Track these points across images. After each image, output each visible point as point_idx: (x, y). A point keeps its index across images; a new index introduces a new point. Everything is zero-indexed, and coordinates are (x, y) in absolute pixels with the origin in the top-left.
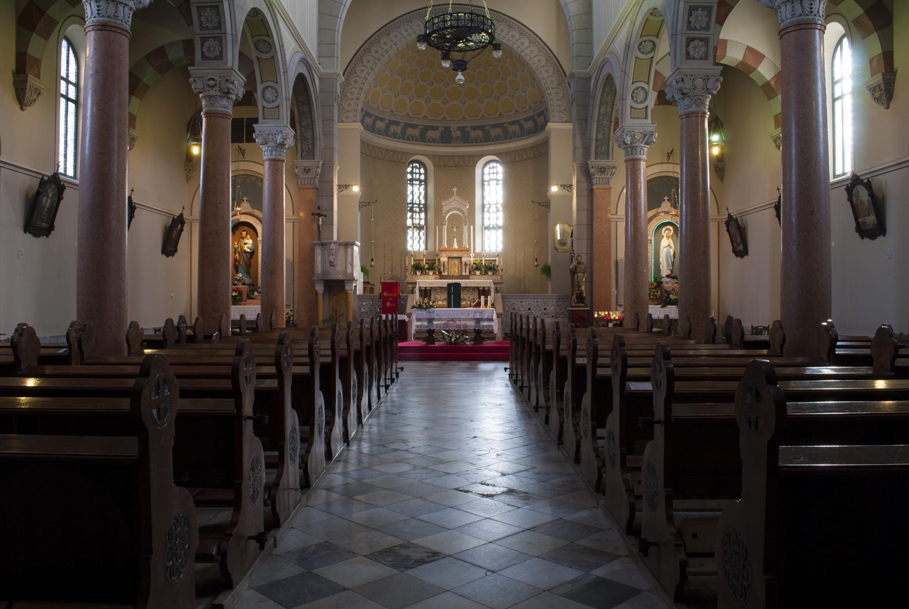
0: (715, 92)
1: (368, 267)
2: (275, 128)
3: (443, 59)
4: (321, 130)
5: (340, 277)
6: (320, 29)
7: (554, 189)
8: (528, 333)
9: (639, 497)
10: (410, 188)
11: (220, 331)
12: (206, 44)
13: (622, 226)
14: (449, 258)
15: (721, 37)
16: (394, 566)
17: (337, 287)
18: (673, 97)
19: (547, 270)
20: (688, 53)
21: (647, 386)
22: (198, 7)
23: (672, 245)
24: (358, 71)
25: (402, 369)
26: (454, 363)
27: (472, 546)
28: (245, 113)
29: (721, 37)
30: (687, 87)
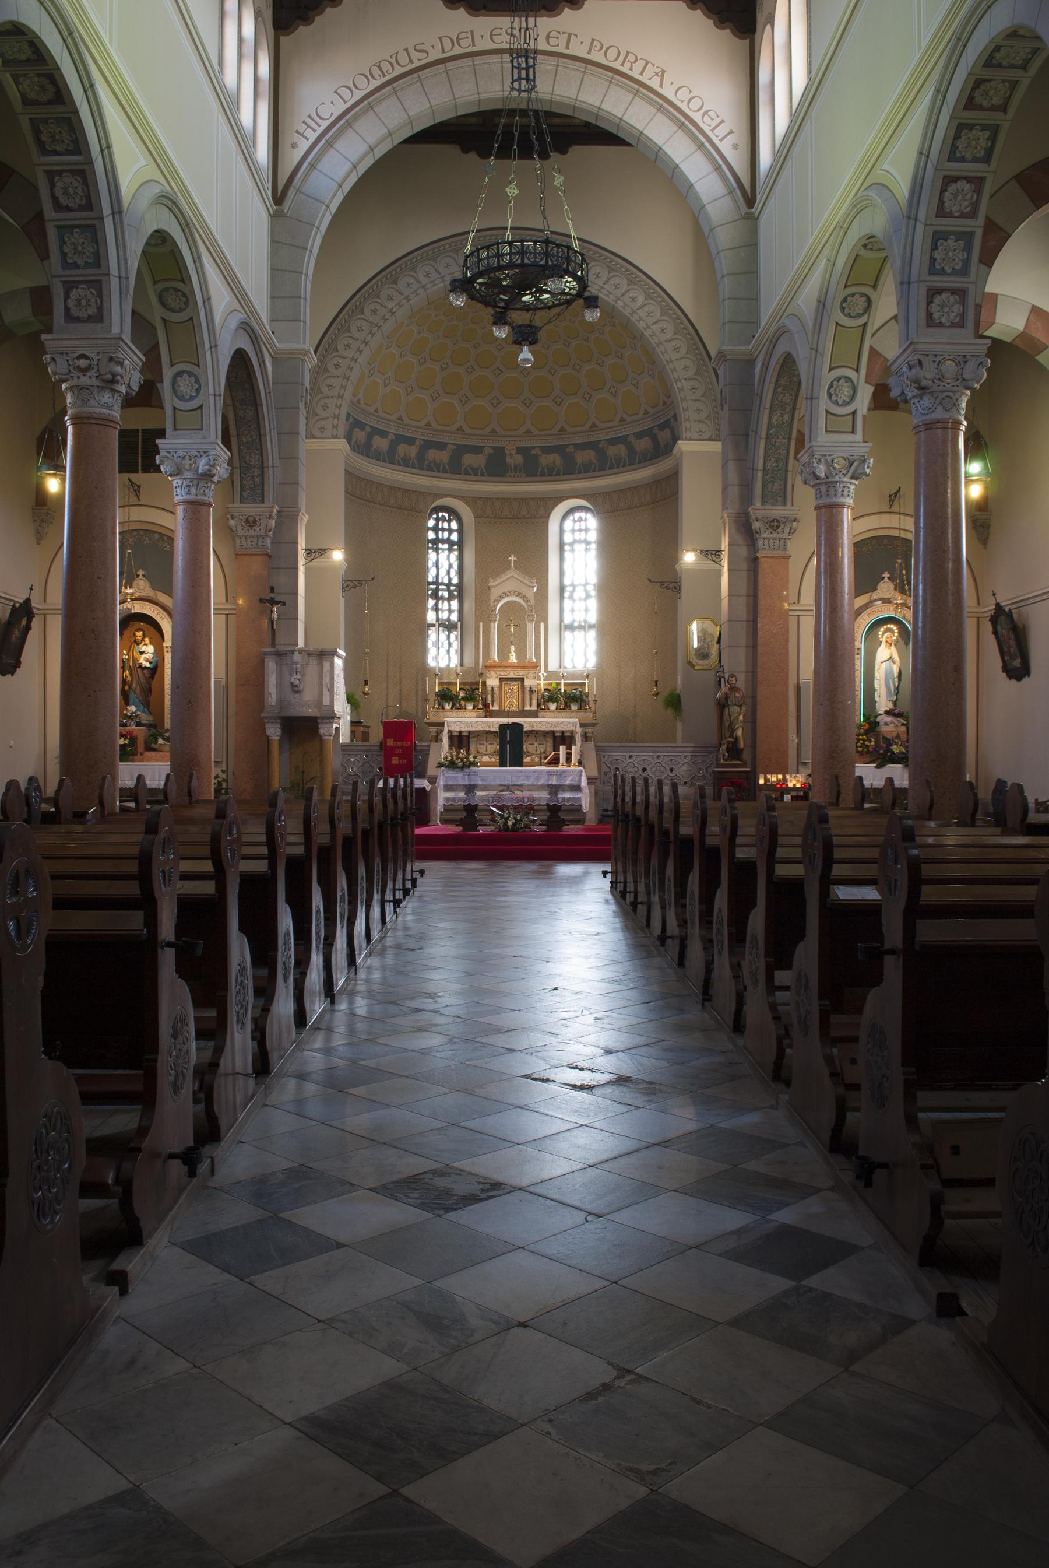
0: (977, 386)
1: (358, 695)
2: (194, 448)
3: (495, 323)
4: (276, 450)
5: (310, 712)
6: (275, 271)
7: (689, 558)
8: (647, 807)
9: (856, 1087)
10: (432, 556)
11: (102, 804)
12: (74, 294)
13: (808, 624)
15: (988, 289)
16: (424, 1207)
17: (304, 729)
18: (903, 393)
19: (674, 702)
20: (930, 316)
21: (871, 894)
22: (58, 227)
23: (896, 657)
24: (341, 347)
25: (422, 872)
26: (511, 863)
27: (559, 1172)
28: (142, 419)
29: (988, 289)
30: (929, 376)
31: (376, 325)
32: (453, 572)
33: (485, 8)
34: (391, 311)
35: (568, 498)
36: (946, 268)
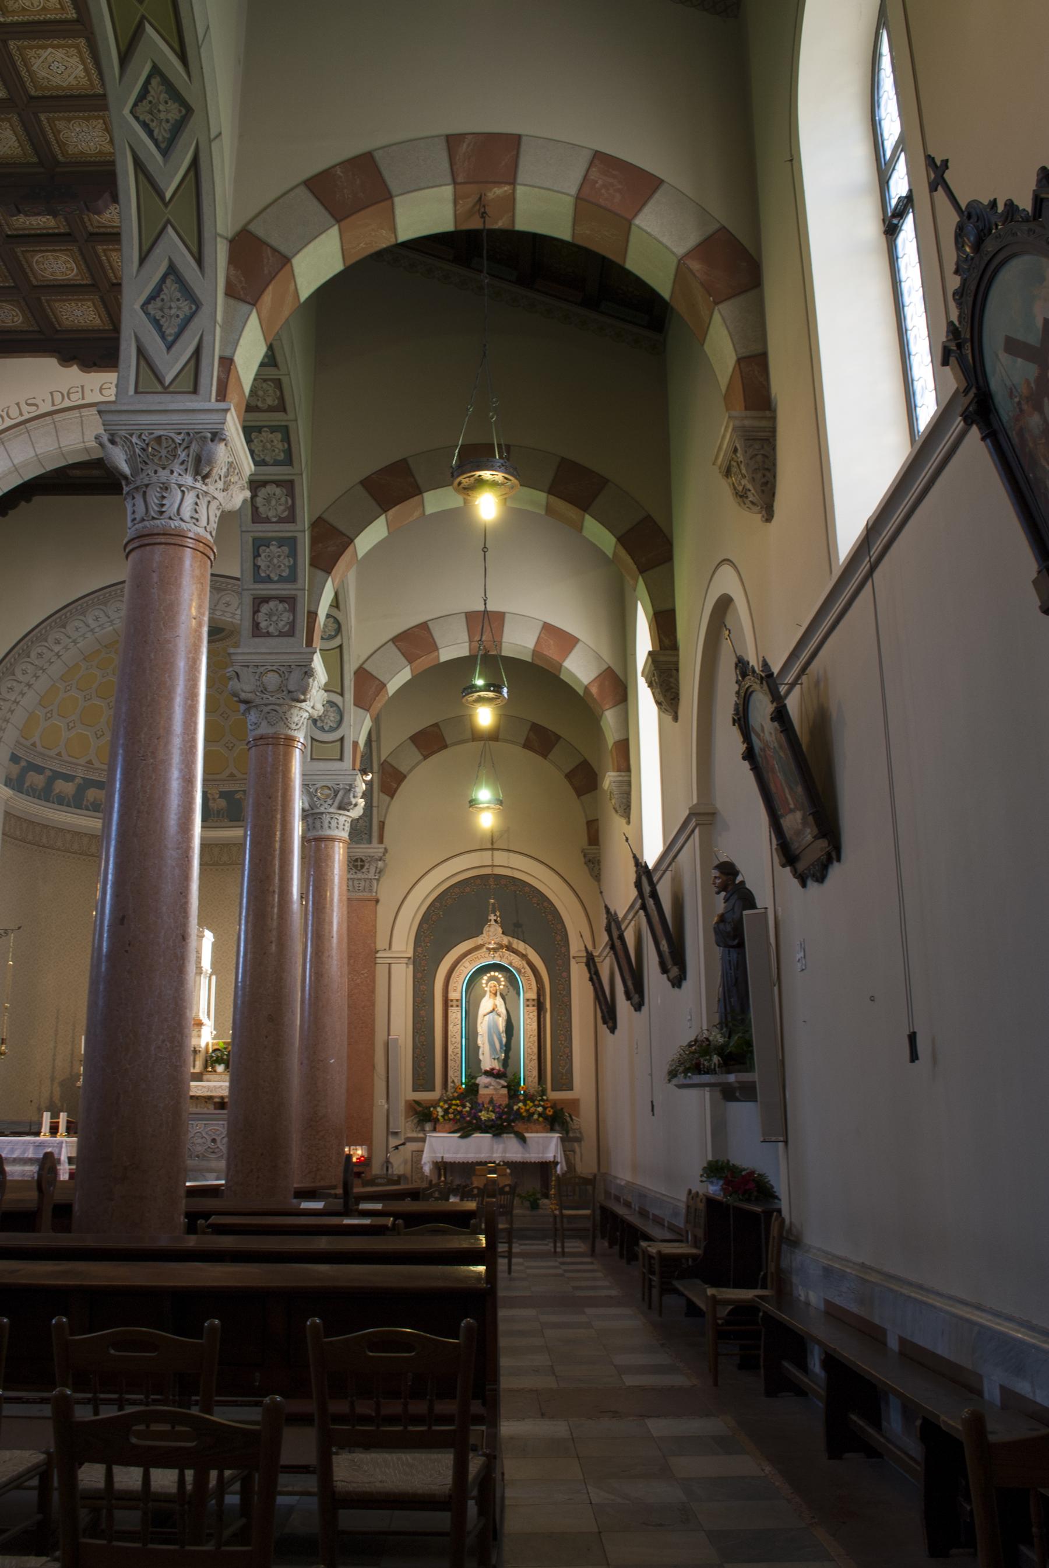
31: (41, 669)
33: (95, 365)
36: (272, 575)
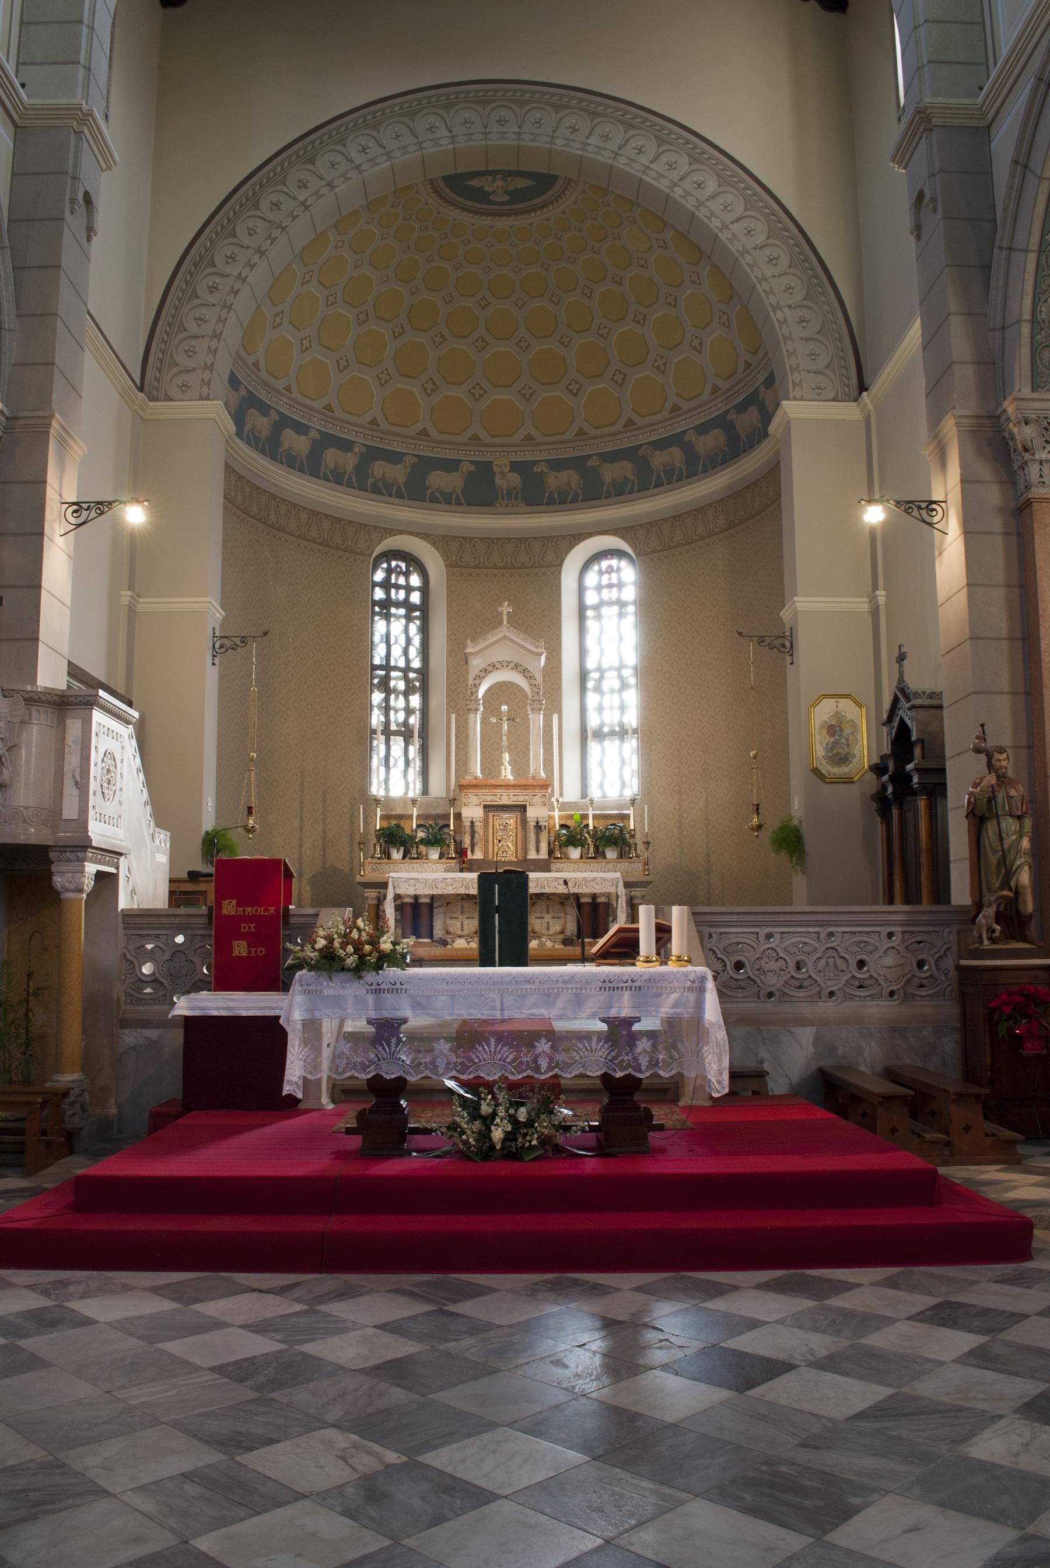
5: (31, 834)
14: (485, 807)
19: (791, 841)
31: (279, 226)
32: (413, 652)
34: (303, 203)
35: (591, 535)
